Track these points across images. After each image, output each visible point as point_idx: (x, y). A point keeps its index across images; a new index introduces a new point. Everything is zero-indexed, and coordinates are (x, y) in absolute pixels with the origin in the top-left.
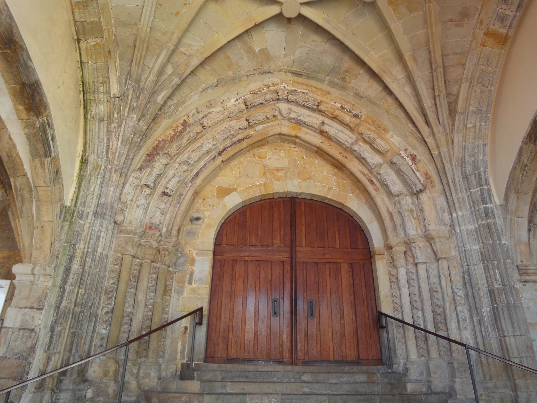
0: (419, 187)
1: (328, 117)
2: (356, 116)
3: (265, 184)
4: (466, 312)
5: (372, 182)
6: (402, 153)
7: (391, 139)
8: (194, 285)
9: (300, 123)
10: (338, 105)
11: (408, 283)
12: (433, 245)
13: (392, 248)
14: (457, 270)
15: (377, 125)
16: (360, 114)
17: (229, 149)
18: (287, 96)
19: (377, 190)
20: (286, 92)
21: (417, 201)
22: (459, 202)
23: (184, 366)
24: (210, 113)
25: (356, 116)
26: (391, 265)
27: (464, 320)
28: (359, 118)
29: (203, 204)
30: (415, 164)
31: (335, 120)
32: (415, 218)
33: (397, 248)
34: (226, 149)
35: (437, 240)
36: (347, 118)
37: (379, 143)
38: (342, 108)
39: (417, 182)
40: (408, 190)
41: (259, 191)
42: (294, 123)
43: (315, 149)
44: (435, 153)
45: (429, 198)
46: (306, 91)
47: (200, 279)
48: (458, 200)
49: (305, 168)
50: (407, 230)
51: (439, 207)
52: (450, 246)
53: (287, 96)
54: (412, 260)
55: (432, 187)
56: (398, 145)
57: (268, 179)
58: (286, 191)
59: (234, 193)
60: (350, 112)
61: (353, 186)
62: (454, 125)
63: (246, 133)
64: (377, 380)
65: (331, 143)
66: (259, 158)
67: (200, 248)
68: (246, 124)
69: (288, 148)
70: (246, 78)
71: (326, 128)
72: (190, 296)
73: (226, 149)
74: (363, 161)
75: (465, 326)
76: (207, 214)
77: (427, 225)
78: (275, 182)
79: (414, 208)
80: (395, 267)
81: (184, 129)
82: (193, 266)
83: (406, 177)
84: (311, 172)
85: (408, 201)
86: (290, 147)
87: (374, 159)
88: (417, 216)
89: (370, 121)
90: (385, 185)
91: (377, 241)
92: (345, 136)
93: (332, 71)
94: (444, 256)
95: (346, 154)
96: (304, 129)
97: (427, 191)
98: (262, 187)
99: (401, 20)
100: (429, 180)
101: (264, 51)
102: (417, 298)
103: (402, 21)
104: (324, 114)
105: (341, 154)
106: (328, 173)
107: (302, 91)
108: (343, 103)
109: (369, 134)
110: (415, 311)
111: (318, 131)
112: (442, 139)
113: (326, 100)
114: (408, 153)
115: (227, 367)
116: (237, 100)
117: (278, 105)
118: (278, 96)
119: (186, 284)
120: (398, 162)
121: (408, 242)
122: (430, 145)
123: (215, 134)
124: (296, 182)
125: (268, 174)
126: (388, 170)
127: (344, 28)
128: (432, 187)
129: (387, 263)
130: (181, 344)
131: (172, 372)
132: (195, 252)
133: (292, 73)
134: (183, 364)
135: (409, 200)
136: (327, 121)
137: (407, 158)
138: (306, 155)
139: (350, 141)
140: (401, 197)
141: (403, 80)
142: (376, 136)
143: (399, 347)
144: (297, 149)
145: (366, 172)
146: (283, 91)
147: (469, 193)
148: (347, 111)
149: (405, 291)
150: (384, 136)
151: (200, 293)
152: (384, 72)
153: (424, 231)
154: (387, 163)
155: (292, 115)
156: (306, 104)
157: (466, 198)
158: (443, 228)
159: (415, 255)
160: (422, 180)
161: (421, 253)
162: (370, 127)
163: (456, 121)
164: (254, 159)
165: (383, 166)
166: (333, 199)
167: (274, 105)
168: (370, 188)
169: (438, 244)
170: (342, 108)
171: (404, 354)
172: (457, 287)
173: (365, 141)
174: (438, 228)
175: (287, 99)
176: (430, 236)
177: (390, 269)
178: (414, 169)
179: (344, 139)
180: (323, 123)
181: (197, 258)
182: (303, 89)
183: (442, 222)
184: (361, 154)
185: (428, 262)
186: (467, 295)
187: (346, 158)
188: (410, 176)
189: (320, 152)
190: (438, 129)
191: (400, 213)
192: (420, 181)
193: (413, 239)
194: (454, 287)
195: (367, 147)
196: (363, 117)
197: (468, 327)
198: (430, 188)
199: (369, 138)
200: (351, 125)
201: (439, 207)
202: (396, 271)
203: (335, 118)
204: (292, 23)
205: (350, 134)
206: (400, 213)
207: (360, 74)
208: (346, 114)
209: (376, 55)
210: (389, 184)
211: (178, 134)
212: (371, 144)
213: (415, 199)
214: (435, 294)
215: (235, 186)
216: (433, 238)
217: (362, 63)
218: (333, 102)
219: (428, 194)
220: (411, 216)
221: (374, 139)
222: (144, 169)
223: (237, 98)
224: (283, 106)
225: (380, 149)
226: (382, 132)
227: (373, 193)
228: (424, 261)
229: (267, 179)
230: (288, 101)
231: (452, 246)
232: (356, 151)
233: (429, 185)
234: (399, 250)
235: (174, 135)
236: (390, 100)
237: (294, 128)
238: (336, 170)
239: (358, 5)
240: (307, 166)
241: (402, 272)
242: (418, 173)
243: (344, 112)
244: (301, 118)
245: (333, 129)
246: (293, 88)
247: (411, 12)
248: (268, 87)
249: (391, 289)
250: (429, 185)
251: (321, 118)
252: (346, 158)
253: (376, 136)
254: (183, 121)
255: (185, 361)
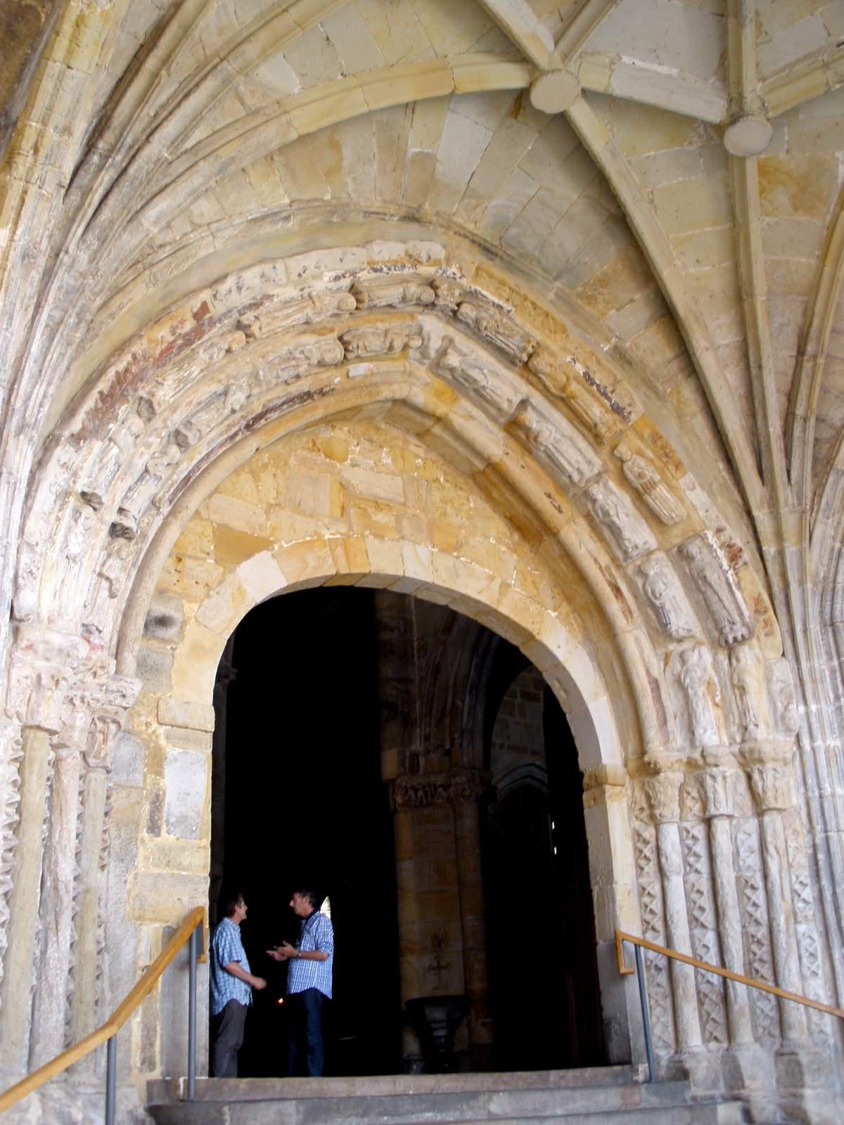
0: (740, 631)
1: (545, 391)
2: (617, 410)
3: (345, 543)
4: (816, 936)
5: (617, 590)
6: (711, 538)
7: (688, 493)
8: (167, 838)
9: (462, 384)
10: (580, 369)
11: (687, 863)
12: (756, 776)
13: (656, 772)
14: (800, 840)
15: (663, 447)
16: (628, 409)
17: (274, 415)
18: (459, 305)
19: (628, 613)
20: (457, 292)
21: (726, 662)
22: (814, 681)
23: (156, 1090)
24: (269, 297)
25: (617, 410)
26: (645, 815)
27: (812, 955)
28: (624, 417)
29: (177, 576)
30: (735, 569)
31: (561, 404)
32: (716, 705)
33: (670, 774)
34: (266, 413)
35: (769, 765)
36: (596, 412)
37: (662, 497)
38: (588, 378)
39: (737, 618)
40: (706, 631)
41: (330, 561)
42: (444, 379)
43: (480, 465)
44: (770, 550)
45: (759, 661)
46: (507, 306)
47: (183, 819)
48: (811, 676)
49: (445, 514)
50: (699, 731)
51: (776, 687)
52: (788, 783)
53: (459, 305)
54: (697, 807)
55: (766, 635)
56: (702, 513)
57: (355, 528)
58: (400, 573)
59: (263, 557)
60: (605, 394)
61: (555, 590)
62: (821, 496)
63: (325, 376)
64: (641, 1101)
65: (529, 460)
66: (327, 456)
67: (180, 721)
68: (339, 353)
69: (400, 443)
70: (360, 218)
71: (530, 418)
72: (157, 871)
73: (266, 413)
74: (606, 533)
75: (814, 968)
76: (191, 609)
77: (751, 727)
78: (372, 543)
79: (716, 680)
80: (655, 821)
81: (198, 332)
82: (160, 774)
83: (714, 599)
84: (460, 527)
85: (703, 660)
86: (406, 442)
87: (638, 534)
88: (723, 699)
89: (647, 433)
90: (653, 606)
91: (606, 746)
92: (577, 456)
93: (565, 271)
94: (780, 805)
95: (560, 500)
96: (465, 404)
97: (754, 641)
98: (340, 551)
99: (767, 215)
100: (762, 618)
101: (426, 160)
102: (706, 901)
103: (767, 219)
104: (535, 380)
105: (549, 496)
106: (499, 540)
107: (496, 300)
108: (594, 366)
109: (641, 466)
110: (698, 932)
111: (503, 420)
112: (790, 522)
113: (554, 347)
114: (723, 539)
115: (273, 1087)
116: (337, 278)
117: (420, 317)
118: (437, 296)
119: (144, 834)
120: (699, 557)
121: (701, 762)
122: (760, 528)
123: (260, 362)
124: (424, 551)
125: (353, 511)
126: (666, 570)
127: (636, 178)
128: (766, 635)
129: (630, 808)
130: (143, 1022)
131: (130, 1112)
132: (162, 730)
133: (473, 241)
134: (150, 1084)
135: (706, 654)
136: (537, 399)
137: (718, 551)
138: (445, 474)
139: (588, 473)
140: (686, 645)
141: (727, 350)
142: (657, 477)
143: (654, 1020)
144: (421, 451)
145: (605, 560)
146: (450, 288)
147: (836, 663)
148: (599, 390)
149: (676, 884)
150: (674, 483)
151: (185, 863)
152: (697, 318)
153: (738, 739)
154: (667, 552)
155: (453, 360)
156: (500, 341)
157: (827, 673)
158: (781, 737)
159: (710, 795)
160: (746, 613)
161: (727, 793)
162: (642, 447)
163: (828, 488)
164: (313, 456)
165: (654, 557)
166: (512, 616)
167: (412, 315)
168: (614, 607)
169: (769, 776)
170: (588, 378)
171: (669, 1036)
172: (802, 879)
173: (623, 480)
174: (771, 737)
175: (455, 312)
176: (756, 755)
177: (637, 824)
178: (731, 581)
179: (573, 461)
180: (524, 403)
181: (172, 751)
182: (500, 297)
183: (782, 721)
184: (612, 512)
185: (736, 815)
186: (821, 899)
187: (560, 511)
188: (724, 599)
189: (490, 480)
190: (786, 495)
191: (680, 684)
192: (741, 614)
193: (716, 756)
194: (794, 878)
195: (626, 499)
196: (633, 417)
197: (820, 972)
198: (762, 637)
199: (640, 476)
200: (603, 430)
201: (776, 687)
202: (653, 831)
203: (563, 401)
204: (519, 117)
205: (590, 453)
206: (680, 684)
207: (632, 301)
208: (593, 396)
209: (691, 275)
210: (668, 606)
211: (180, 342)
212: (639, 495)
213: (723, 657)
214: (748, 892)
215: (265, 534)
216: (761, 761)
217: (647, 275)
218: (565, 358)
219: (757, 650)
220: (709, 698)
221: (652, 485)
222: (85, 439)
223: (340, 273)
224: (435, 327)
225: (664, 512)
226: (672, 468)
227: (620, 621)
228: (730, 811)
229: (350, 528)
230: (454, 316)
231: (792, 782)
232: (594, 501)
233: (760, 630)
234: (673, 777)
235: (170, 347)
236: (688, 392)
237: (439, 394)
238: (516, 537)
239: (690, 143)
240: (450, 510)
241: (671, 835)
242: (738, 594)
243: (590, 392)
244: (475, 374)
245: (552, 427)
246: (474, 287)
247: (796, 209)
248: (416, 262)
249: (639, 876)
250: (760, 630)
251: (525, 390)
252: (560, 511)
253: (657, 477)
254: (199, 305)
255: (156, 1074)
